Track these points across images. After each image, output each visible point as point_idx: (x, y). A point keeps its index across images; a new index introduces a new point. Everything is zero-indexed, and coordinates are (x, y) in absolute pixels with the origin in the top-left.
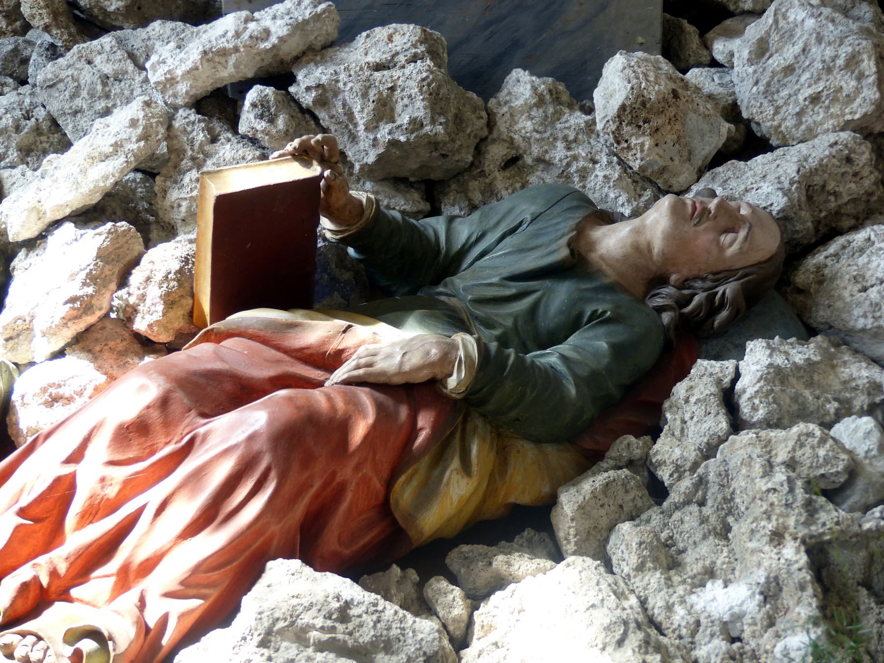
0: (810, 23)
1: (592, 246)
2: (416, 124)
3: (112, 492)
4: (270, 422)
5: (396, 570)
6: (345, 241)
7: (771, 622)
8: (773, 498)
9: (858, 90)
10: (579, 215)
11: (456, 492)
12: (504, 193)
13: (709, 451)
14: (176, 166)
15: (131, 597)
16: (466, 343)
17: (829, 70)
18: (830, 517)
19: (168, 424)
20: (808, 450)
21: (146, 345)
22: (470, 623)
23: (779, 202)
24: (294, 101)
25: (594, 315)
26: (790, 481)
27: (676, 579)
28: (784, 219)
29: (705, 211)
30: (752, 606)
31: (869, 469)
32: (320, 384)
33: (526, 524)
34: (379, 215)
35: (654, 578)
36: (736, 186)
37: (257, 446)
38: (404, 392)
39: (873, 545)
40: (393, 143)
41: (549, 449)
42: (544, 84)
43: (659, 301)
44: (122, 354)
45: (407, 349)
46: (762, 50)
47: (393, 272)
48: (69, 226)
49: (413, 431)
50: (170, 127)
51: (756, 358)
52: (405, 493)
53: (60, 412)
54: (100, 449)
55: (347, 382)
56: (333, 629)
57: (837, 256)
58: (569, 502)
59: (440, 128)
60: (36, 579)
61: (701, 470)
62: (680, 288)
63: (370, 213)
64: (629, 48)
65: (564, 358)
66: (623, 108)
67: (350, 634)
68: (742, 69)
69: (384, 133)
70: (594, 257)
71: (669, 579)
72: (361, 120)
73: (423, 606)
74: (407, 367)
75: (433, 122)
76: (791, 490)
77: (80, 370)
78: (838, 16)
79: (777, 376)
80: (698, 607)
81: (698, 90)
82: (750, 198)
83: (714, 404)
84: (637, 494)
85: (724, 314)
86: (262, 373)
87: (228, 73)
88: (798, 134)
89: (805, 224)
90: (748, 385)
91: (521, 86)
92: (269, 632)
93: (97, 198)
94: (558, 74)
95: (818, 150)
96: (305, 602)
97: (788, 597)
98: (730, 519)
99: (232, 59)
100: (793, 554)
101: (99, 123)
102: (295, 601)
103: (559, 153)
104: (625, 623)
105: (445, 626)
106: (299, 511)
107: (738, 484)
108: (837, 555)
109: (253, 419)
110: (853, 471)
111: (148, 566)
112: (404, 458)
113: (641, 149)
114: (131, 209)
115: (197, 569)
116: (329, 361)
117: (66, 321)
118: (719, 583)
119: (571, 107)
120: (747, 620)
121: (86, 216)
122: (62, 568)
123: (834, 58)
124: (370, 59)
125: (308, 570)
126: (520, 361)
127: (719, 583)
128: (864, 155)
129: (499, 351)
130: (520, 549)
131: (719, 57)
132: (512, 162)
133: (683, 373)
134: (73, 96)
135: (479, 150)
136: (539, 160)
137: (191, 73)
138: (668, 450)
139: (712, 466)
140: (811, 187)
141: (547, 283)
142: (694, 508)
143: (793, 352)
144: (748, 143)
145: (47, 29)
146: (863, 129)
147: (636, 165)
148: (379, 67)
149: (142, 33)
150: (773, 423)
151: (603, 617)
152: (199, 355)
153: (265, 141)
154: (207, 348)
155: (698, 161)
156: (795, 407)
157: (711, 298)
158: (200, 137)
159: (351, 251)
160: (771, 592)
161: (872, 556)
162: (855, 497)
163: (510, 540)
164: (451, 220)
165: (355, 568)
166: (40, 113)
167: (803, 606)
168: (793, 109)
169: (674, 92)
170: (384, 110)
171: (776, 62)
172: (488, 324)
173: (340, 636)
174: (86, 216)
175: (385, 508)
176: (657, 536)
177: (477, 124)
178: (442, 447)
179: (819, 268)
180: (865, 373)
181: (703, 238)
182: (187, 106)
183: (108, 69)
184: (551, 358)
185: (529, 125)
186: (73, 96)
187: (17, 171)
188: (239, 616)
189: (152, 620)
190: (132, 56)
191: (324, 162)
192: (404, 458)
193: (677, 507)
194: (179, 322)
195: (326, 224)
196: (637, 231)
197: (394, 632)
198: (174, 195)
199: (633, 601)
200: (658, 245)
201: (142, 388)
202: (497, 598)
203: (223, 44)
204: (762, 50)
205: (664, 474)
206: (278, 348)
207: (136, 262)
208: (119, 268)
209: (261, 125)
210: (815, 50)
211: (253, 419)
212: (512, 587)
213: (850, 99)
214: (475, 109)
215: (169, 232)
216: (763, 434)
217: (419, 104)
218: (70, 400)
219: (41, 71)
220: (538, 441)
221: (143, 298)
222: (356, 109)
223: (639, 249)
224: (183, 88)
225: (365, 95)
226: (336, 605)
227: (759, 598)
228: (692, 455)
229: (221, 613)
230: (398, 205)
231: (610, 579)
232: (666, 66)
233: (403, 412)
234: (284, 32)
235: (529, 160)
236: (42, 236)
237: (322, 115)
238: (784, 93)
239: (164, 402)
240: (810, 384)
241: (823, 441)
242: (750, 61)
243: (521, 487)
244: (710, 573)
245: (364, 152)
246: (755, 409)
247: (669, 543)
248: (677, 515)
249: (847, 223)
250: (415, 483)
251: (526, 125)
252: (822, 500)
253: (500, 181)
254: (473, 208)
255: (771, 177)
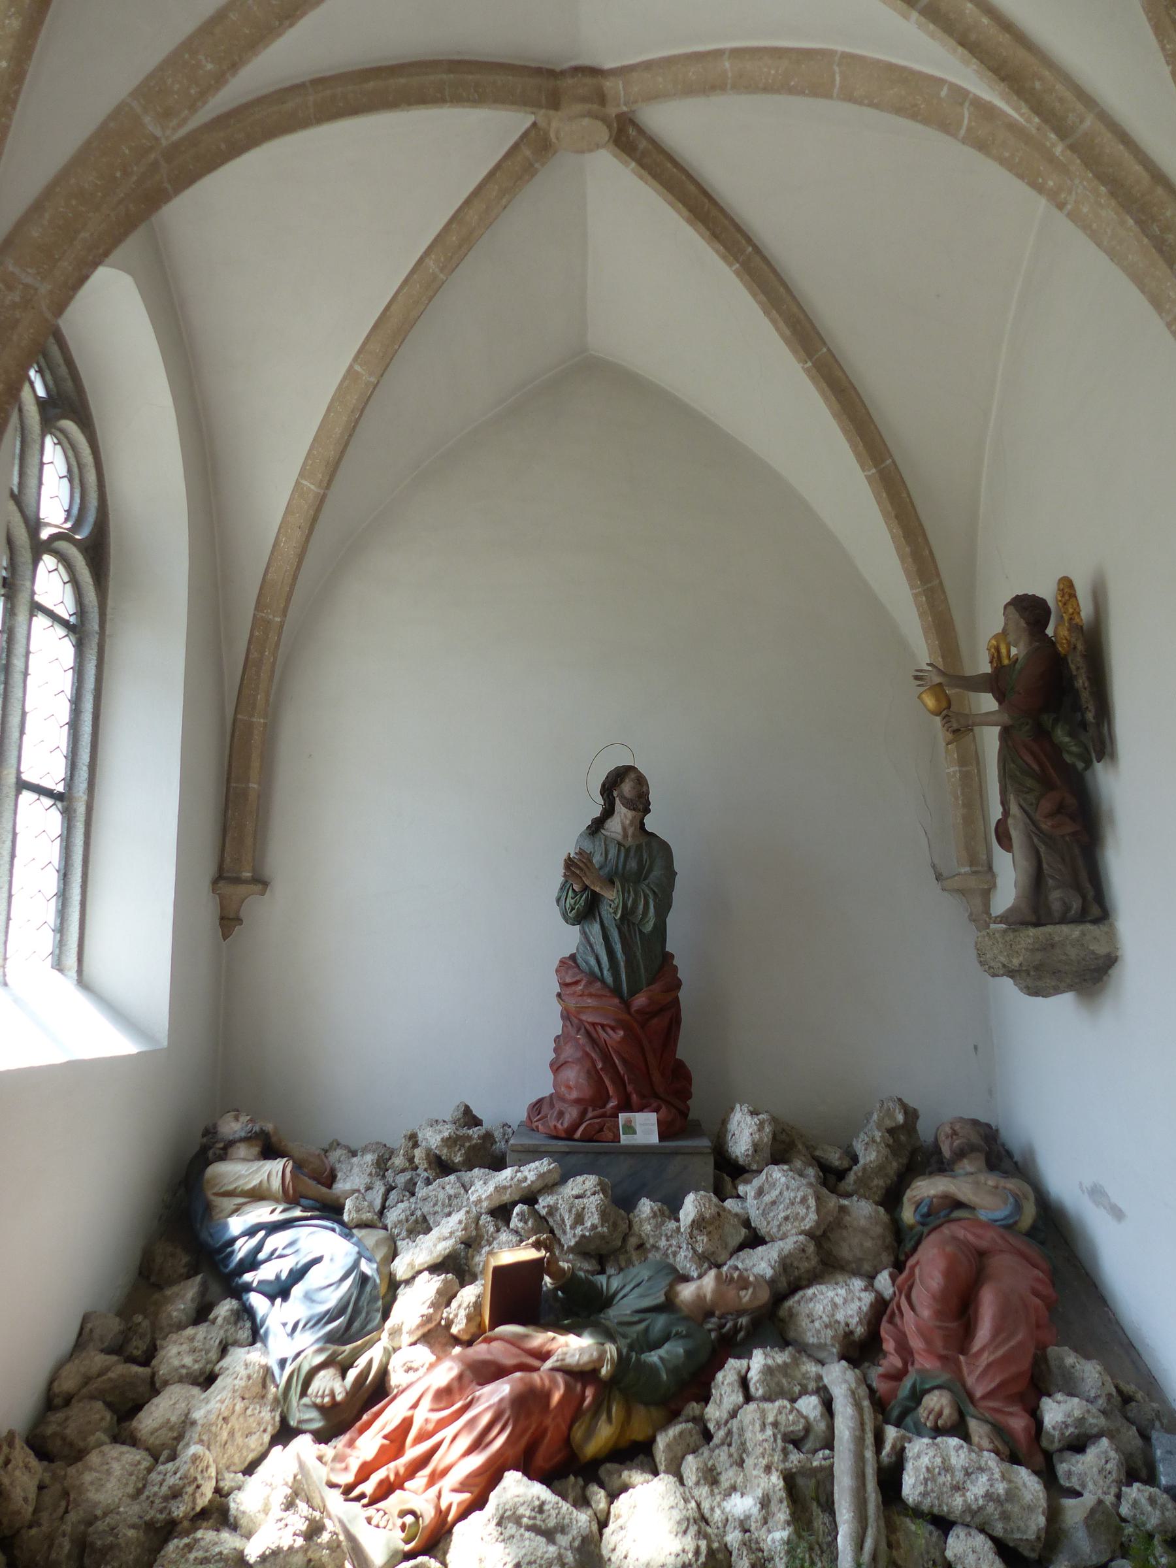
0: (783, 1179)
1: (677, 1294)
2: (594, 1227)
3: (430, 1427)
4: (511, 1391)
5: (572, 1478)
6: (556, 1289)
7: (765, 1522)
8: (766, 1445)
9: (807, 1215)
10: (671, 1278)
11: (604, 1434)
12: (636, 1263)
13: (733, 1414)
14: (479, 1244)
15: (434, 1491)
16: (611, 1349)
17: (793, 1204)
18: (795, 1458)
19: (462, 1389)
20: (784, 1416)
21: (456, 1341)
22: (609, 1513)
23: (769, 1273)
24: (536, 1212)
25: (677, 1333)
26: (774, 1435)
27: (716, 1491)
28: (772, 1282)
29: (732, 1278)
30: (755, 1510)
31: (816, 1428)
32: (537, 1369)
33: (636, 1453)
34: (574, 1275)
35: (704, 1490)
36: (749, 1263)
37: (504, 1405)
38: (580, 1375)
39: (819, 1476)
40: (583, 1236)
41: (653, 1410)
42: (656, 1206)
43: (709, 1326)
44: (445, 1345)
45: (582, 1351)
46: (760, 1193)
47: (579, 1306)
48: (426, 1273)
49: (583, 1399)
50: (477, 1224)
51: (758, 1360)
52: (578, 1433)
53: (412, 1376)
54: (426, 1403)
55: (554, 1369)
56: (535, 1518)
57: (799, 1302)
58: (662, 1442)
59: (605, 1229)
60: (388, 1477)
61: (729, 1425)
62: (719, 1318)
63: (569, 1275)
64: (697, 1190)
65: (661, 1358)
66: (693, 1221)
67: (544, 1521)
68: (751, 1201)
69: (579, 1231)
70: (678, 1301)
71: (712, 1491)
72: (568, 1223)
73: (583, 1502)
74: (581, 1362)
75: (602, 1226)
76: (775, 1440)
77: (423, 1354)
78: (797, 1177)
79: (768, 1371)
80: (727, 1510)
81: (730, 1211)
82: (756, 1270)
83: (736, 1386)
84: (696, 1438)
85: (742, 1334)
86: (509, 1361)
87: (506, 1197)
88: (779, 1236)
89: (783, 1284)
90: (754, 1375)
91: (646, 1207)
92: (502, 1517)
93: (440, 1259)
94: (664, 1201)
95: (788, 1245)
96: (521, 1500)
97: (774, 1507)
98: (744, 1456)
99: (509, 1191)
100: (776, 1480)
101: (444, 1220)
102: (516, 1499)
103: (663, 1243)
104: (688, 1520)
105: (595, 1514)
106: (523, 1442)
107: (748, 1435)
108: (801, 1481)
109: (501, 1390)
110: (808, 1429)
111: (445, 1472)
112: (578, 1414)
113: (702, 1242)
114: (455, 1267)
115: (469, 1476)
116: (544, 1356)
117: (418, 1327)
118: (739, 1494)
119: (670, 1218)
120: (753, 1519)
121: (434, 1269)
122: (402, 1471)
123: (795, 1197)
124: (574, 1193)
125: (525, 1479)
126: (638, 1360)
127: (739, 1494)
128: (811, 1248)
129: (628, 1354)
130: (637, 1468)
131: (741, 1194)
132: (640, 1246)
133: (721, 1367)
134: (435, 1205)
135: (625, 1239)
136: (653, 1246)
137: (489, 1197)
138: (714, 1412)
139: (734, 1424)
140: (785, 1265)
141: (653, 1315)
142: (725, 1448)
143: (777, 1356)
144: (755, 1240)
145: (425, 1170)
146: (810, 1234)
147: (700, 1250)
148: (577, 1197)
149: (469, 1174)
150: (768, 1398)
151: (676, 1515)
152: (480, 1350)
153: (522, 1232)
154: (484, 1346)
155: (730, 1249)
156: (777, 1389)
157: (735, 1325)
158: (492, 1229)
159: (560, 1293)
160: (765, 1503)
161: (818, 1483)
162: (809, 1445)
163: (632, 1460)
164: (609, 1277)
165: (547, 1479)
166: (419, 1213)
167: (782, 1514)
168: (776, 1223)
169: (719, 1214)
170: (579, 1219)
171: (767, 1199)
172: (624, 1336)
173: (538, 1522)
174: (434, 1269)
175: (567, 1440)
176: (706, 1465)
177: (624, 1226)
178: (600, 1405)
179: (790, 1308)
180: (814, 1369)
181: (731, 1292)
182: (487, 1213)
183: (452, 1192)
184: (653, 1357)
185: (649, 1227)
186: (435, 1205)
187: (405, 1242)
188: (1020, 594)
189: (444, 1506)
190: (463, 1186)
191: (547, 1249)
192: (578, 1414)
193: (718, 1446)
194: (473, 1329)
195: (547, 1279)
196: (699, 1288)
197: (567, 1521)
198: (477, 1259)
199: (693, 1504)
200: (709, 1296)
201: (451, 1369)
202: (623, 1496)
203: (505, 1183)
204: (760, 1193)
205: (711, 1426)
206: (519, 1348)
207: (455, 1296)
208: (446, 1297)
209: (520, 1225)
210: (786, 1193)
211: (501, 1390)
212: (631, 1491)
213: (803, 1219)
214: (623, 1219)
215: (473, 1278)
216: (761, 1405)
217: (596, 1216)
218: (416, 1370)
219: (421, 1191)
220: (647, 1404)
221: (456, 1316)
222: (566, 1218)
223: (700, 1298)
224: (485, 1204)
225: (570, 1211)
226: (537, 1503)
227: (759, 1506)
228: (725, 1416)
229: (478, 1503)
230: (584, 1267)
231: (681, 1489)
232: (715, 1199)
233: (579, 1387)
234: (533, 1178)
235: (648, 1246)
236: (413, 1278)
237: (550, 1220)
238: (772, 1215)
239: (460, 1377)
240: (786, 1375)
241: (791, 1411)
242: (755, 1198)
243: (638, 1432)
244: (734, 1488)
245: (569, 1239)
246: (757, 1389)
247: (712, 1469)
248: (717, 1451)
249: (804, 1283)
250: (583, 1427)
251: (647, 1228)
252: (791, 1447)
253: (634, 1256)
254: (621, 1270)
255: (766, 1259)
